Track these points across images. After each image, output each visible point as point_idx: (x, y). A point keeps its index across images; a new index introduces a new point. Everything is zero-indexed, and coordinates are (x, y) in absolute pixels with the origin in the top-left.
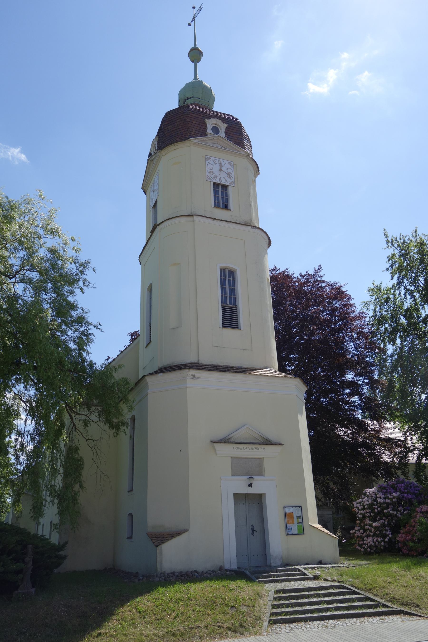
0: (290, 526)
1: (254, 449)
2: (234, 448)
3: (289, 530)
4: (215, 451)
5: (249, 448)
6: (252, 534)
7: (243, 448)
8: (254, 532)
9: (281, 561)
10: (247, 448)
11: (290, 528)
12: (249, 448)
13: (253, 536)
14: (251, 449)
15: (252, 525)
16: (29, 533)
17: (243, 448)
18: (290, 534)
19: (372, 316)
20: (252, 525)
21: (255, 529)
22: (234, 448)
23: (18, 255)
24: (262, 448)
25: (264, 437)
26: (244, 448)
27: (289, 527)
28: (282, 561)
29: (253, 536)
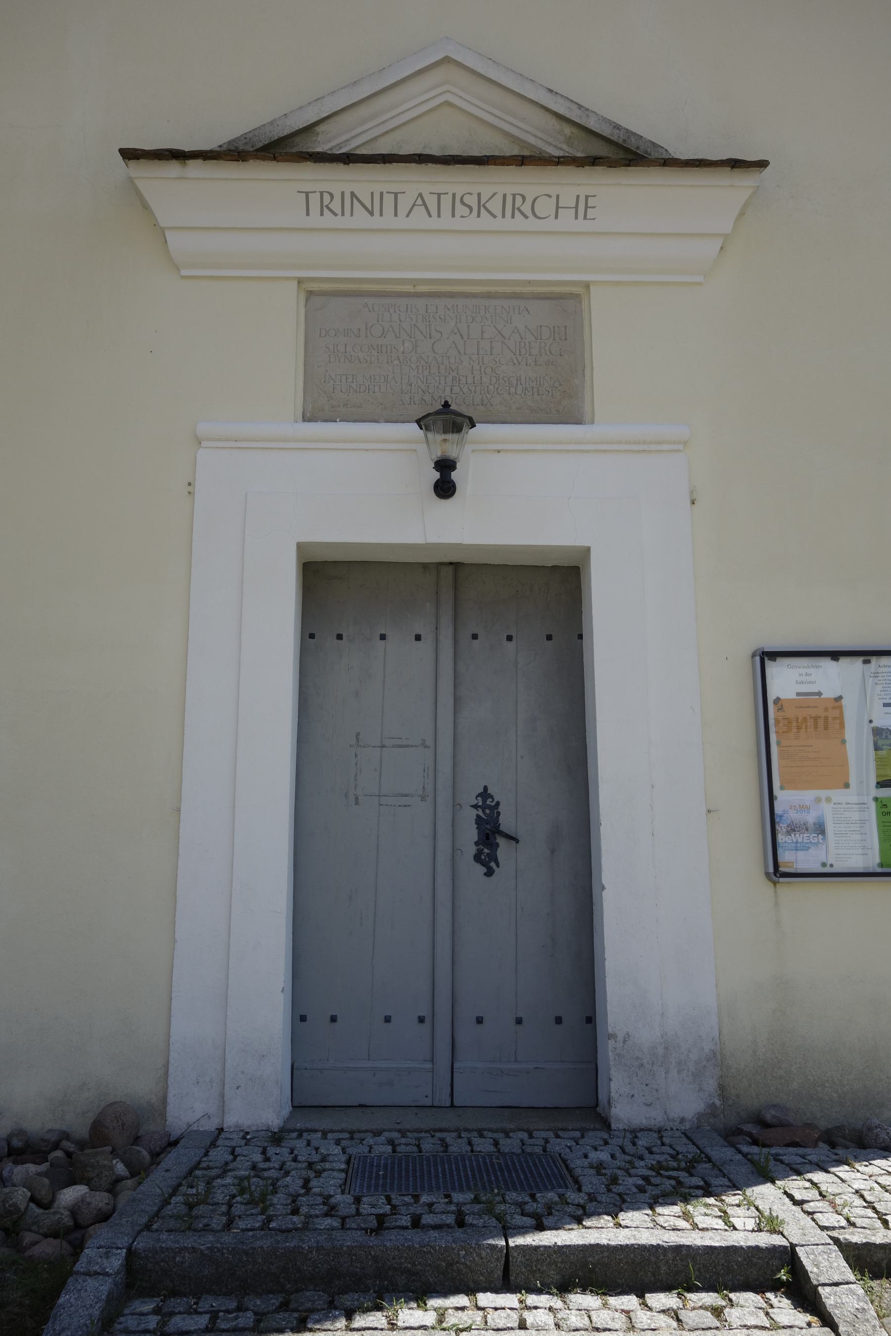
0: (804, 808)
1: (495, 205)
2: (315, 199)
3: (799, 837)
4: (161, 233)
5: (446, 201)
6: (477, 858)
7: (389, 200)
8: (494, 847)
9: (711, 1085)
10: (432, 202)
11: (811, 818)
12: (446, 201)
13: (489, 873)
14: (461, 209)
15: (485, 794)
16: (604, 1245)
17: (389, 200)
18: (802, 867)
19: (732, 1145)
20: (485, 794)
21: (506, 822)
22: (315, 199)
23: (609, 1195)
24: (567, 200)
25: (592, 124)
26: (405, 203)
27: (794, 816)
28: (722, 1088)
29: (489, 873)
